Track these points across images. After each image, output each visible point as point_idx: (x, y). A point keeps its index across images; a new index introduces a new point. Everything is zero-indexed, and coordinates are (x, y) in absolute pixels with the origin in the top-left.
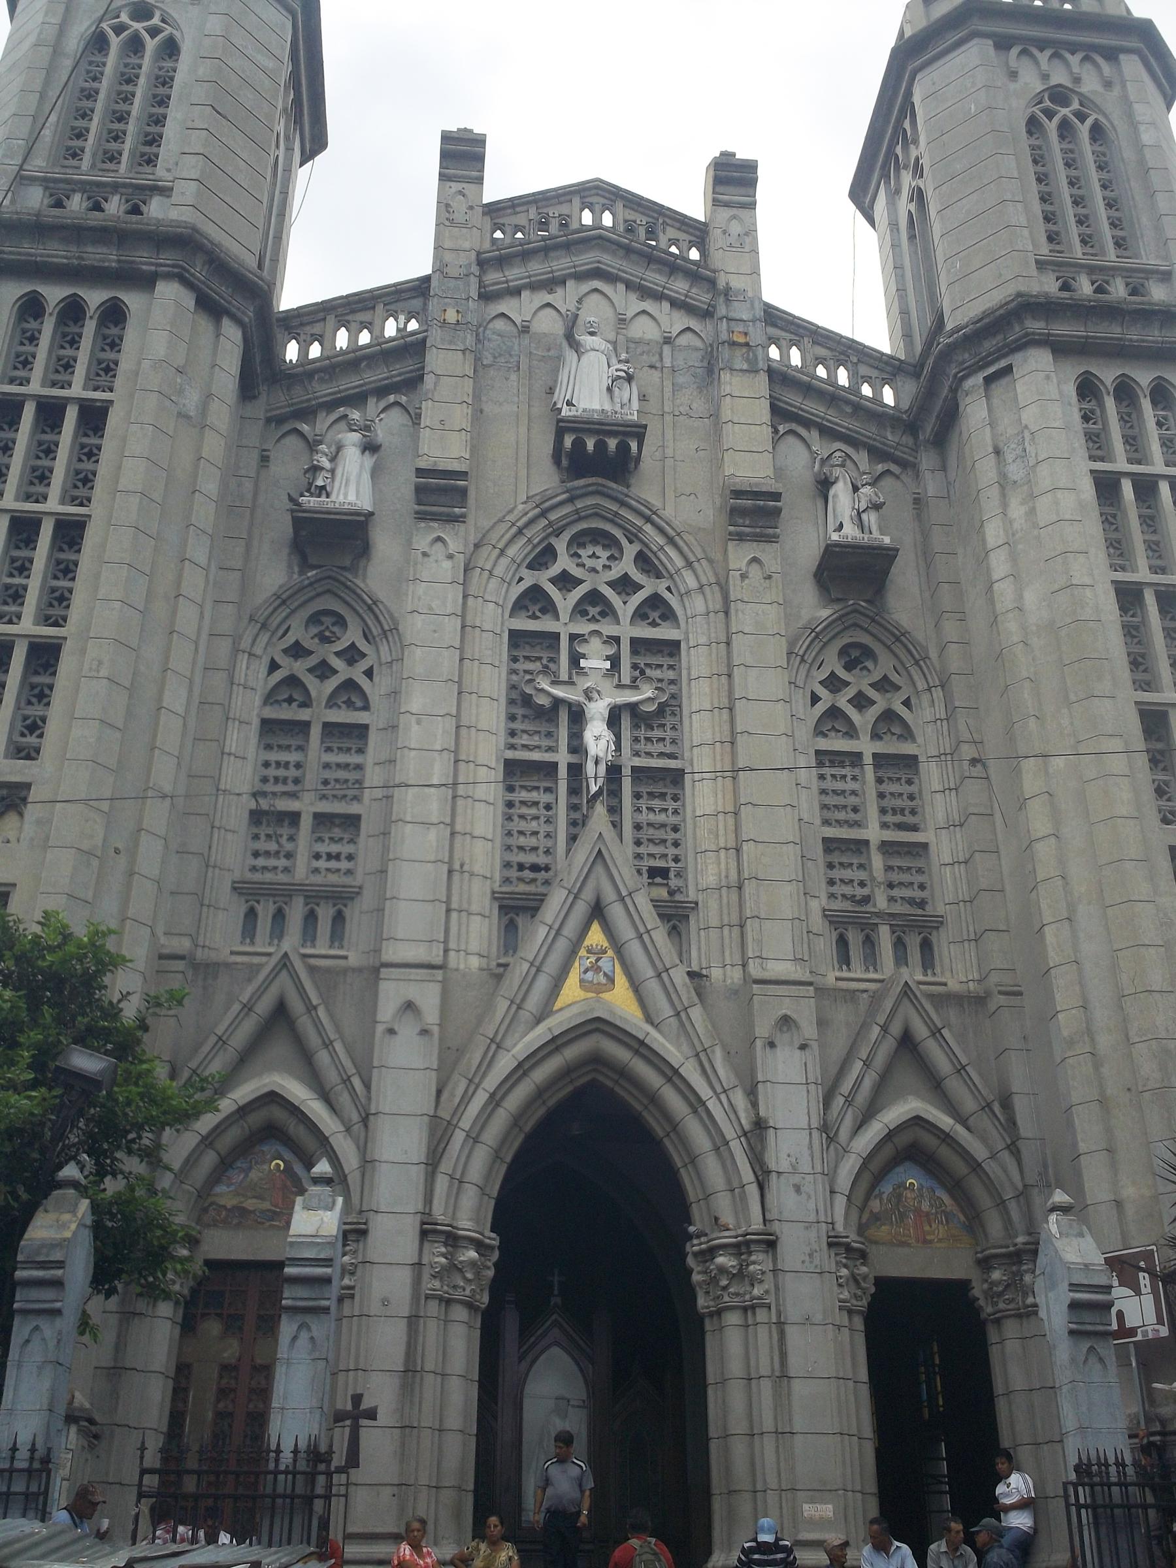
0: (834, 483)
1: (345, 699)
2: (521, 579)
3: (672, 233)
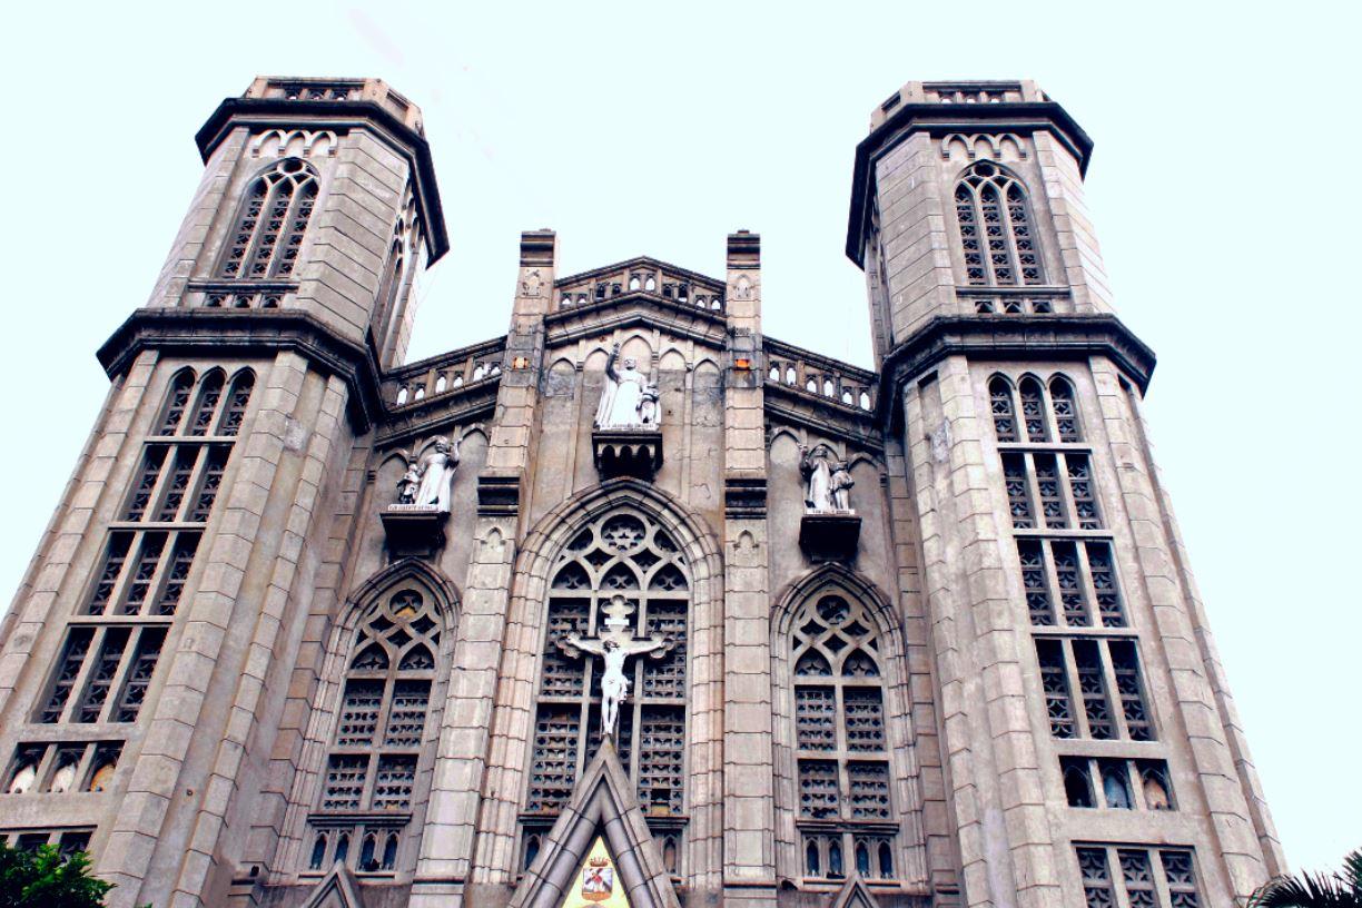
0: (815, 470)
1: (416, 660)
2: (563, 557)
3: (699, 291)
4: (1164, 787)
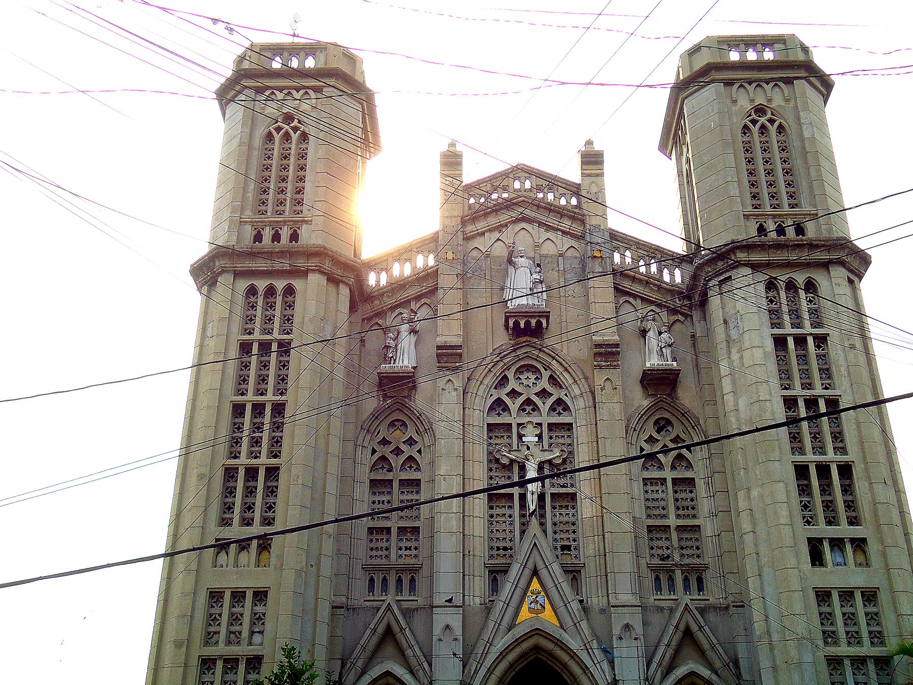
4: (864, 552)
